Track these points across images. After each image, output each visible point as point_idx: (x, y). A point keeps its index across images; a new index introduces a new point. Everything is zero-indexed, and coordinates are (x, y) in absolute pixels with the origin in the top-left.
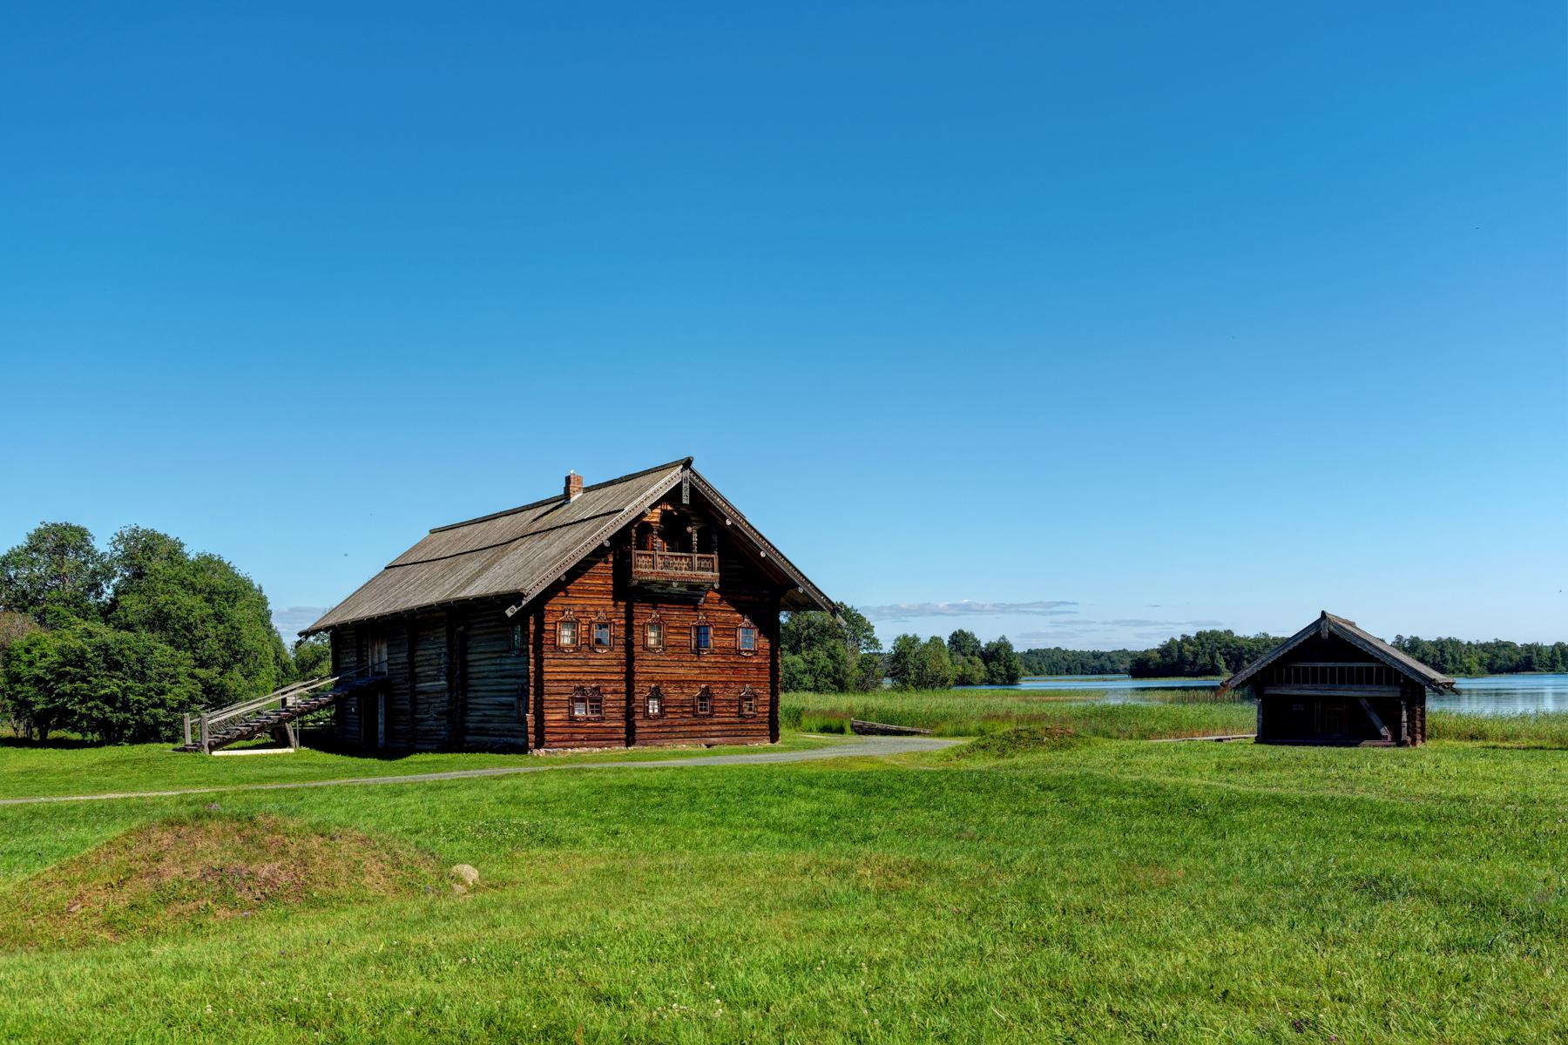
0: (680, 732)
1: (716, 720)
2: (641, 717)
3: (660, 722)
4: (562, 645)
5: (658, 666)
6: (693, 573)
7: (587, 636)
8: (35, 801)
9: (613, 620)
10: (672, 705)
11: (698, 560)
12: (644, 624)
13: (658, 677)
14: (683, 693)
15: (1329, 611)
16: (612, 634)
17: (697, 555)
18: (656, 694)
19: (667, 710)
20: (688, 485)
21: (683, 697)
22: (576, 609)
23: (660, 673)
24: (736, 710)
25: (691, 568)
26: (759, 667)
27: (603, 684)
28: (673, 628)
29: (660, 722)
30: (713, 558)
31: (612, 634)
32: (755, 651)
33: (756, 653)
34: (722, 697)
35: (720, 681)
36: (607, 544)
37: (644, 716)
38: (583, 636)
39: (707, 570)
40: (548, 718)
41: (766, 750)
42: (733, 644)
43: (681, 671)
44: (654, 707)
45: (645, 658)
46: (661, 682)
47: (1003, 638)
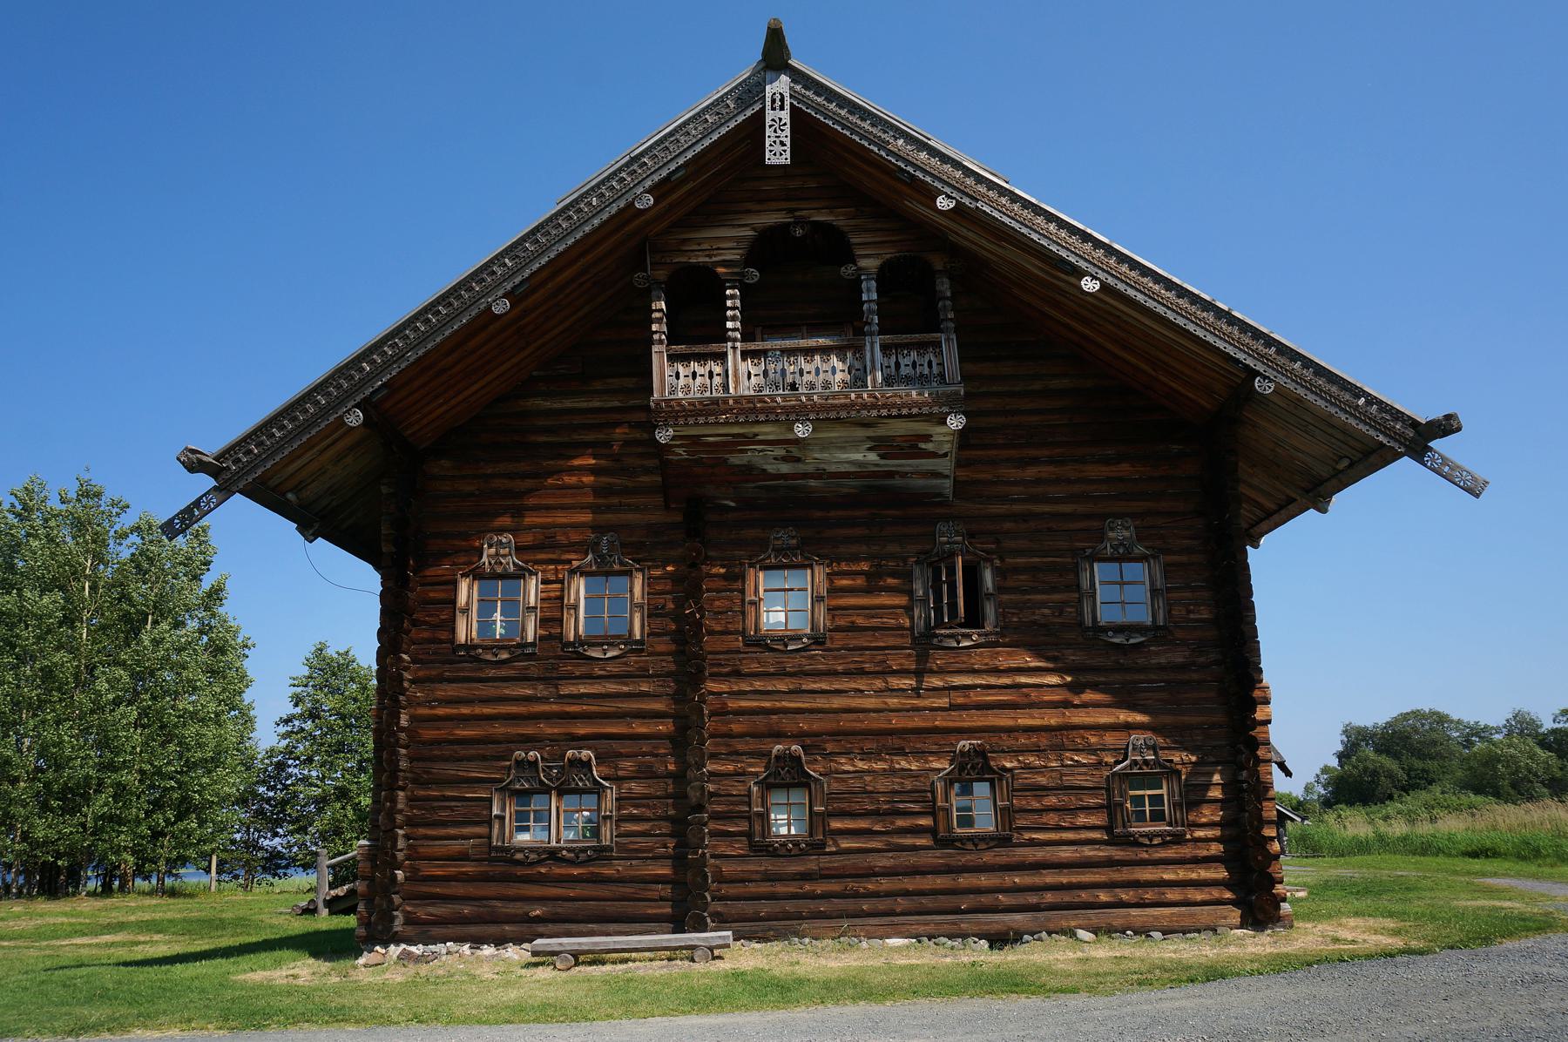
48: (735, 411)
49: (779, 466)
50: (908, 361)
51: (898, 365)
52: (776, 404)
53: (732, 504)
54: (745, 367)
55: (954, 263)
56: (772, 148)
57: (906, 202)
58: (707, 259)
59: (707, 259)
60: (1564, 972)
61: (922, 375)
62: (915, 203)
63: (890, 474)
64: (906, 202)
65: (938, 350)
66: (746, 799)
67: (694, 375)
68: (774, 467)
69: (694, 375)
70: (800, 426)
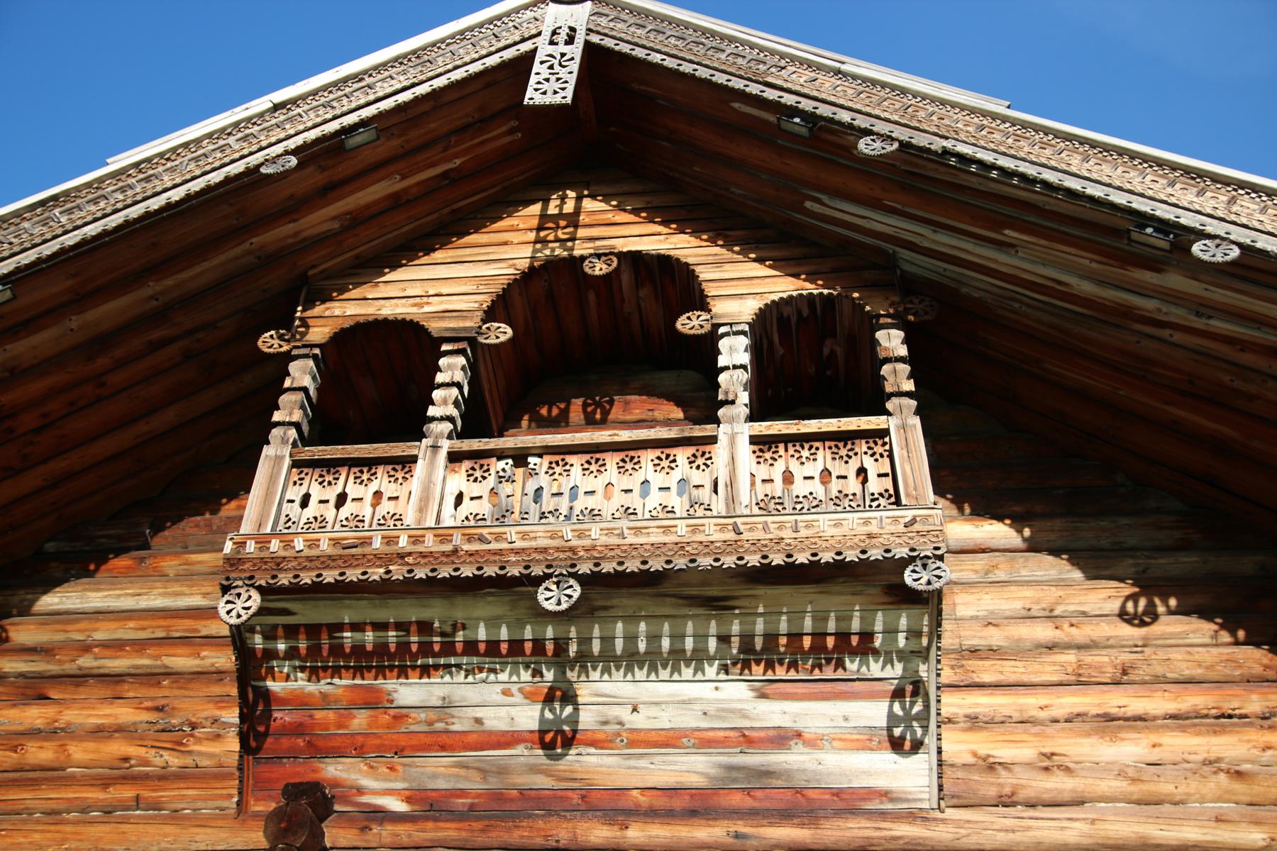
30: (884, 433)
48: (410, 560)
49: (513, 711)
50: (814, 469)
51: (788, 478)
52: (504, 546)
53: (398, 806)
54: (458, 481)
55: (911, 302)
56: (593, 461)
57: (808, 204)
58: (415, 310)
59: (415, 310)
60: (1, 719)
62: (824, 198)
63: (782, 738)
64: (808, 204)
65: (879, 449)
66: (927, 789)
67: (341, 499)
68: (503, 712)
69: (341, 499)
70: (554, 587)
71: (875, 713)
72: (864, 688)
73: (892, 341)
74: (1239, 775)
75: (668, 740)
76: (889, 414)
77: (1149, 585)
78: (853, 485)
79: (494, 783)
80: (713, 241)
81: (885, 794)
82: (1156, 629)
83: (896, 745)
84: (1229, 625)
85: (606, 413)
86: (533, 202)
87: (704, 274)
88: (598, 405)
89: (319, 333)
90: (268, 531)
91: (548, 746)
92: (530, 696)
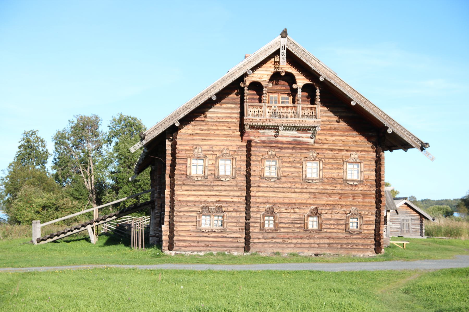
0: (291, 243)
1: (323, 235)
2: (257, 230)
3: (273, 235)
4: (192, 174)
5: (273, 191)
6: (297, 119)
7: (213, 168)
8: (336, 269)
9: (235, 156)
10: (286, 222)
11: (302, 109)
12: (262, 159)
13: (271, 200)
14: (295, 213)
15: (280, 34)
16: (234, 166)
17: (301, 106)
18: (271, 212)
19: (280, 225)
20: (285, 51)
21: (294, 216)
22: (205, 148)
23: (273, 197)
24: (344, 227)
25: (296, 115)
26: (365, 195)
27: (224, 205)
28: (286, 162)
29: (273, 235)
30: (315, 108)
31: (234, 166)
32: (360, 181)
33: (361, 182)
34: (329, 217)
35: (328, 204)
36: (214, 98)
37: (260, 230)
38: (210, 168)
39: (311, 116)
40: (180, 229)
41: (369, 260)
42: (340, 175)
43: (293, 195)
44: (269, 223)
45: (262, 185)
46: (274, 204)
47: (435, 158)
53: (259, 142)
61: (310, 115)
71: (309, 135)
72: (309, 133)
73: (318, 91)
74: (343, 141)
75: (288, 137)
76: (316, 104)
77: (340, 117)
78: (312, 114)
79: (269, 140)
80: (297, 71)
81: (308, 142)
82: (340, 123)
83: (311, 138)
84: (347, 124)
85: (278, 84)
86: (273, 58)
87: (296, 77)
88: (277, 82)
89: (248, 84)
90: (276, 151)
91: (275, 137)
92: (274, 132)
